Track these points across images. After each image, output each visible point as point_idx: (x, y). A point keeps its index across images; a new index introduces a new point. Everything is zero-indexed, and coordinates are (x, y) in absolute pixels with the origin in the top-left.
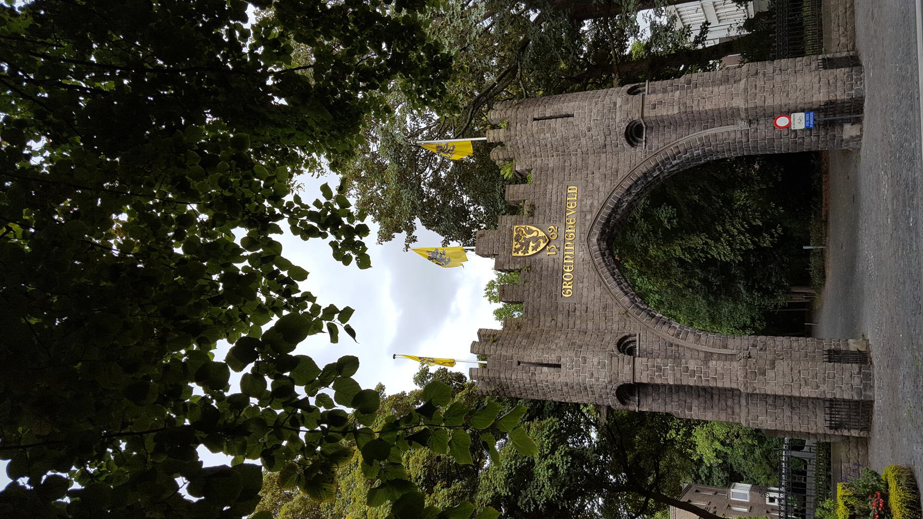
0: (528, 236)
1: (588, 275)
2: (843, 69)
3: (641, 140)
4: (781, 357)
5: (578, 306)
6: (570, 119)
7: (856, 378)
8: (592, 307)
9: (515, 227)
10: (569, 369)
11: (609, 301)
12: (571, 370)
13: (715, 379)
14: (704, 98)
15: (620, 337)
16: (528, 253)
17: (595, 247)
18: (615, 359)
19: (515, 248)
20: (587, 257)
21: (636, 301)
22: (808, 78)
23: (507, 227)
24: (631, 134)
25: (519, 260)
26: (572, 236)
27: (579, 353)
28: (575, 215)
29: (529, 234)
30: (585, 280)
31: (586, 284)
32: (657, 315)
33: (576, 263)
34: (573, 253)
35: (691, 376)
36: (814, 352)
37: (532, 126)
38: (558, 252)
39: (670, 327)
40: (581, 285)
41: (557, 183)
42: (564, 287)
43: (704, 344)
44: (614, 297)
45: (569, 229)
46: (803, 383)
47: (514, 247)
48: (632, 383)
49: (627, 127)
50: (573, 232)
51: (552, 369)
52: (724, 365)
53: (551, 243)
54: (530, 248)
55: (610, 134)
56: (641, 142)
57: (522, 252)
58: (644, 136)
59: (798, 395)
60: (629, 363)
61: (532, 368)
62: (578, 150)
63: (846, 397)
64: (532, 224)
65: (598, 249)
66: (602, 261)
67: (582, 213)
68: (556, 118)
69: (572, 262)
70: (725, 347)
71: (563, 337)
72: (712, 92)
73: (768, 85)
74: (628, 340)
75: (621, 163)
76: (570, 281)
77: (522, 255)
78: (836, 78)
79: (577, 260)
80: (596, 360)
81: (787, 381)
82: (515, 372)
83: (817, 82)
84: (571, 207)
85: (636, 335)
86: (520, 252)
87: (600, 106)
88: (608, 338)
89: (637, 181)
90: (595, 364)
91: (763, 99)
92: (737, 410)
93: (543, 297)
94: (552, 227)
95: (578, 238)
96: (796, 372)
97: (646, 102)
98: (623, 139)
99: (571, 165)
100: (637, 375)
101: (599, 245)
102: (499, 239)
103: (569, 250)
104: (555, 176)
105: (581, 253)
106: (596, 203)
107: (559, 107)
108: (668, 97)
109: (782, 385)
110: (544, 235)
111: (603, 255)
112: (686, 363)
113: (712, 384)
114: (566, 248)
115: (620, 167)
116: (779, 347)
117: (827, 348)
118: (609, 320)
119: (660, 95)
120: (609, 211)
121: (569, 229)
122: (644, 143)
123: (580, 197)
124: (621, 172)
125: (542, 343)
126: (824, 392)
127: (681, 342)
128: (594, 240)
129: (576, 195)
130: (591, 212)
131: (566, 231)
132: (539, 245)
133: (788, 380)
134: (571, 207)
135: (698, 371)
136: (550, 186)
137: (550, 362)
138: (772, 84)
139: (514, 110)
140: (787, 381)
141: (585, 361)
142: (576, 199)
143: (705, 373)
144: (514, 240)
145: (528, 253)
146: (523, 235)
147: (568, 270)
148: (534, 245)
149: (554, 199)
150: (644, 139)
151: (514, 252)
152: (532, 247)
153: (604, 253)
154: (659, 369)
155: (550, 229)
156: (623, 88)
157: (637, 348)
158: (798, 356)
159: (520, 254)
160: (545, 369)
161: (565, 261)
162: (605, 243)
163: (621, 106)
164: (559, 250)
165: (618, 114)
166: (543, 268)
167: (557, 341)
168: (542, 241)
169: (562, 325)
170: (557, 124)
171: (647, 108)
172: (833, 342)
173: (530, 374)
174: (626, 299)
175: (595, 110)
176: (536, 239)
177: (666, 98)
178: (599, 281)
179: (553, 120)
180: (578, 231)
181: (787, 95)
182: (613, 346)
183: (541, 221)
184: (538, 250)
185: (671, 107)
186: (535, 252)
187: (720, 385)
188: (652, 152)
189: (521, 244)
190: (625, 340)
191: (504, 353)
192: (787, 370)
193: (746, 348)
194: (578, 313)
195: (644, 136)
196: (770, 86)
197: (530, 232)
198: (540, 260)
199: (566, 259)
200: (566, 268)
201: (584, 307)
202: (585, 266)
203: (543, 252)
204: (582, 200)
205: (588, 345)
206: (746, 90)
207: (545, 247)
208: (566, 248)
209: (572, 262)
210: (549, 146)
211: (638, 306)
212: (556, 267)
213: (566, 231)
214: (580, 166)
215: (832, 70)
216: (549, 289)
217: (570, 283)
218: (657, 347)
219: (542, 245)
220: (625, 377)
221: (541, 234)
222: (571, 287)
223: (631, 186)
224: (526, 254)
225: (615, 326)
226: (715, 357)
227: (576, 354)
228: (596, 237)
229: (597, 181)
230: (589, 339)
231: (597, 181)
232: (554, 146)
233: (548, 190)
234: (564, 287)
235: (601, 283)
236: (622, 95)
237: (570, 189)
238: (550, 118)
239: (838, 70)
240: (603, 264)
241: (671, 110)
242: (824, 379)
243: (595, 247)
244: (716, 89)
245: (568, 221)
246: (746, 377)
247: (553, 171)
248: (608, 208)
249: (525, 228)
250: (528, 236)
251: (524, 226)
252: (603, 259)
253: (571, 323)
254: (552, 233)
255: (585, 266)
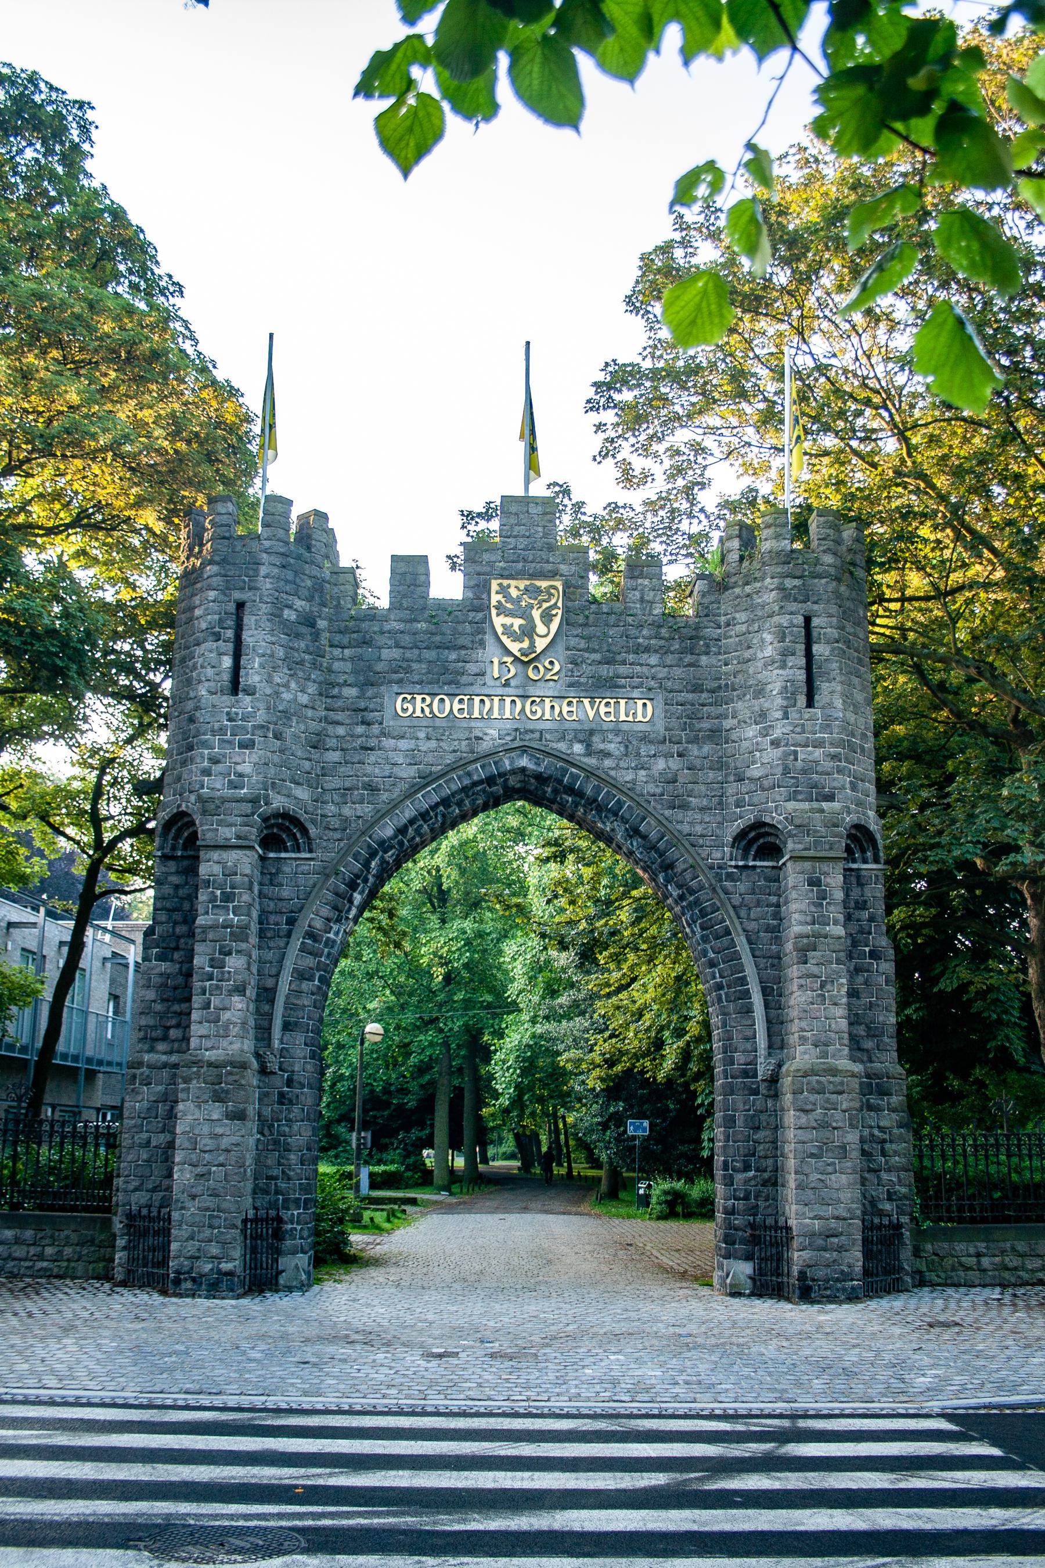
0: (536, 614)
1: (445, 751)
2: (860, 1263)
3: (751, 857)
4: (266, 1132)
5: (376, 729)
6: (802, 700)
7: (210, 1266)
8: (372, 759)
9: (559, 585)
10: (228, 713)
11: (385, 796)
12: (225, 717)
13: (207, 1006)
14: (822, 986)
15: (303, 817)
16: (498, 615)
17: (507, 762)
18: (247, 808)
19: (509, 586)
20: (485, 746)
21: (386, 852)
22: (846, 1196)
23: (562, 567)
24: (760, 836)
25: (484, 596)
26: (534, 713)
27: (258, 732)
28: (582, 717)
29: (542, 616)
30: (433, 744)
31: (425, 746)
32: (355, 895)
33: (473, 724)
34: (496, 715)
35: (212, 960)
36: (277, 1193)
37: (791, 613)
38: (498, 683)
39: (328, 920)
40: (422, 735)
41: (660, 676)
42: (419, 698)
43: (293, 987)
44: (395, 805)
45: (553, 707)
46: (199, 1170)
47: (513, 583)
48: (198, 843)
49: (773, 826)
50: (543, 714)
51: (226, 677)
52: (235, 1024)
53: (520, 666)
54: (508, 621)
55: (763, 789)
56: (745, 857)
57: (499, 602)
58: (758, 863)
59: (177, 1160)
60: (238, 837)
61: (230, 634)
62: (735, 721)
63: (174, 1246)
64: (566, 621)
65: (502, 770)
66: (475, 778)
67: (587, 735)
68: (809, 668)
69: (476, 715)
70: (287, 1027)
71: (304, 699)
72: (835, 1004)
73: (838, 1118)
74: (298, 835)
75: (698, 816)
76: (431, 712)
77: (494, 602)
78: (840, 1249)
79: (479, 724)
80: (246, 768)
81: (204, 1142)
82: (222, 597)
83: (836, 1213)
84: (603, 709)
85: (311, 851)
86: (499, 597)
87: (828, 765)
88: (302, 793)
89: (657, 851)
90: (239, 768)
91: (809, 1107)
92: (161, 1046)
93: (396, 653)
94: (557, 667)
95: (531, 726)
96: (221, 1159)
97: (825, 867)
98: (750, 818)
99: (703, 705)
100: (215, 855)
101: (514, 772)
102: (533, 549)
103: (502, 708)
104: (678, 672)
105: (494, 733)
106: (608, 763)
107: (833, 674)
108: (836, 913)
109: (196, 1132)
110: (539, 650)
111: (490, 780)
112: (238, 952)
113: (197, 1001)
114: (508, 700)
115: (690, 813)
116: (287, 1129)
117: (285, 1215)
118: (344, 795)
119: (839, 895)
120: (589, 791)
121: (553, 707)
122: (741, 863)
123: (625, 727)
124: (680, 815)
125: (286, 653)
126: (183, 1208)
127: (296, 943)
128: (524, 762)
129: (630, 719)
130: (589, 752)
131: (547, 700)
132: (517, 639)
133: (207, 1143)
134: (603, 709)
135: (223, 973)
136: (654, 660)
137: (242, 672)
138: (840, 1124)
139: (832, 571)
140: (204, 1142)
141: (243, 745)
142: (623, 717)
143: (218, 987)
144: (528, 583)
145: (498, 615)
146: (540, 603)
147: (456, 706)
148: (516, 628)
149: (622, 670)
150: (751, 863)
151: (500, 585)
152: (512, 625)
153: (496, 784)
154: (228, 898)
155: (551, 663)
156: (871, 814)
157: (283, 855)
158: (269, 1162)
159: (495, 598)
160: (227, 662)
161: (477, 699)
162: (518, 785)
163: (822, 811)
164: (504, 685)
165: (806, 805)
166: (463, 652)
167: (293, 685)
168: (526, 644)
169: (333, 697)
170: (791, 672)
171: (814, 868)
172: (299, 1228)
173: (217, 629)
174: (389, 832)
175: (818, 753)
176: (528, 631)
177: (832, 908)
178: (431, 773)
179: (803, 662)
180: (548, 726)
181: (812, 1155)
182: (278, 802)
183: (573, 642)
184: (504, 638)
185: (809, 919)
186: (499, 630)
187: (195, 1016)
188: (721, 880)
189: (519, 599)
190: (300, 830)
191: (263, 570)
192: (225, 1143)
193: (285, 1066)
194: (360, 729)
195: (758, 863)
196: (837, 1121)
197: (547, 618)
198: (482, 644)
199: (482, 701)
200: (461, 701)
201: (372, 742)
202: (464, 743)
203: (499, 651)
204: (617, 732)
205: (282, 751)
206: (834, 1072)
207: (509, 653)
208: (508, 700)
209: (476, 715)
210: (747, 654)
211: (373, 855)
212: (464, 679)
213: (547, 700)
214: (697, 726)
215: (860, 1242)
216: (415, 666)
217: (427, 710)
218: (286, 893)
219: (514, 647)
220: (207, 829)
221: (541, 644)
222: (418, 713)
223: (644, 837)
224: (494, 612)
225: (330, 809)
226: (266, 1008)
227: (263, 727)
228: (531, 766)
229: (661, 764)
230: (299, 753)
231: (661, 764)
232: (744, 666)
233: (645, 656)
234: (419, 698)
235: (427, 779)
236: (849, 813)
237: (645, 705)
238: (809, 655)
239: (859, 1255)
240: (467, 782)
241: (802, 918)
242: (207, 1209)
243: (507, 762)
244: (840, 1012)
245: (570, 704)
246: (210, 1064)
247: (690, 665)
248: (597, 789)
249: (555, 605)
250: (536, 614)
251: (560, 604)
252: (481, 782)
253: (339, 716)
254: (542, 669)
255: (464, 743)
